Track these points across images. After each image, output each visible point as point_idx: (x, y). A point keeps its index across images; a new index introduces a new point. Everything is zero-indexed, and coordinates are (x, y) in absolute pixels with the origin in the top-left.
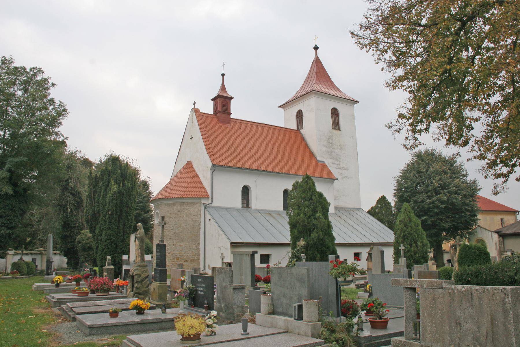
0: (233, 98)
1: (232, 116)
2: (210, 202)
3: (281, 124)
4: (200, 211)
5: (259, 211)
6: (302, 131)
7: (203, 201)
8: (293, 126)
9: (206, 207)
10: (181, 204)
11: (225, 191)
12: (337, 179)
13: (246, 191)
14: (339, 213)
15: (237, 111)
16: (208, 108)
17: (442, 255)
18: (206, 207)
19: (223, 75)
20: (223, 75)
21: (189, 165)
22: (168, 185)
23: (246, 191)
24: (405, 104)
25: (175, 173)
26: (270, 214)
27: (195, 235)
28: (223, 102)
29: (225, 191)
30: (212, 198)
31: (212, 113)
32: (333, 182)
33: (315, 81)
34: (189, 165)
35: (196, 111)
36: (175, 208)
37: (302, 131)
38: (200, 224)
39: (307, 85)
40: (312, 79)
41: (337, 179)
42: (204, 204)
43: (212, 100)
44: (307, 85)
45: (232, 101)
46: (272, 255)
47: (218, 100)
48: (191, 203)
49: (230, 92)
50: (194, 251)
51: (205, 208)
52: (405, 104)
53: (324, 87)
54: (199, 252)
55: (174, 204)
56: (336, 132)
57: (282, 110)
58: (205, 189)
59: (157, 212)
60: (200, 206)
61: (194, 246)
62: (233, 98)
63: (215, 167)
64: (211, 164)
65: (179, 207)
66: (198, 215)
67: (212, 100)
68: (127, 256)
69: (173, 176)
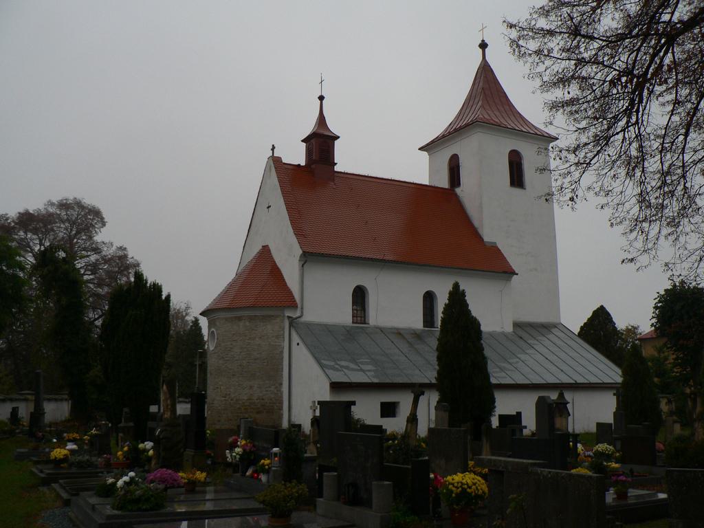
0: (339, 137)
1: (337, 168)
2: (298, 314)
3: (423, 178)
4: (283, 329)
5: (382, 330)
6: (458, 190)
7: (288, 313)
8: (444, 183)
9: (292, 322)
10: (251, 318)
11: (324, 298)
12: (517, 274)
13: (360, 296)
14: (521, 333)
15: (346, 160)
16: (296, 155)
17: (440, 375)
18: (292, 322)
19: (321, 98)
20: (321, 98)
21: (265, 251)
22: (231, 286)
23: (360, 296)
24: (298, 344)
25: (243, 265)
26: (400, 334)
27: (272, 369)
28: (321, 143)
29: (324, 298)
30: (302, 308)
31: (303, 163)
32: (509, 279)
33: (480, 103)
34: (265, 251)
35: (276, 162)
36: (241, 324)
37: (458, 190)
38: (282, 352)
39: (468, 110)
40: (476, 101)
41: (517, 274)
42: (289, 317)
43: (302, 141)
44: (468, 110)
45: (337, 142)
46: (401, 404)
47: (313, 141)
48: (270, 316)
49: (333, 126)
50: (272, 396)
51: (291, 325)
52: (298, 344)
53: (498, 114)
54: (282, 397)
55: (240, 319)
56: (517, 191)
57: (425, 154)
58: (293, 298)
59: (213, 332)
60: (283, 321)
61: (272, 388)
62: (339, 137)
63: (309, 257)
64: (301, 252)
65: (247, 324)
66: (280, 337)
67: (302, 141)
68: (157, 406)
69: (240, 271)
